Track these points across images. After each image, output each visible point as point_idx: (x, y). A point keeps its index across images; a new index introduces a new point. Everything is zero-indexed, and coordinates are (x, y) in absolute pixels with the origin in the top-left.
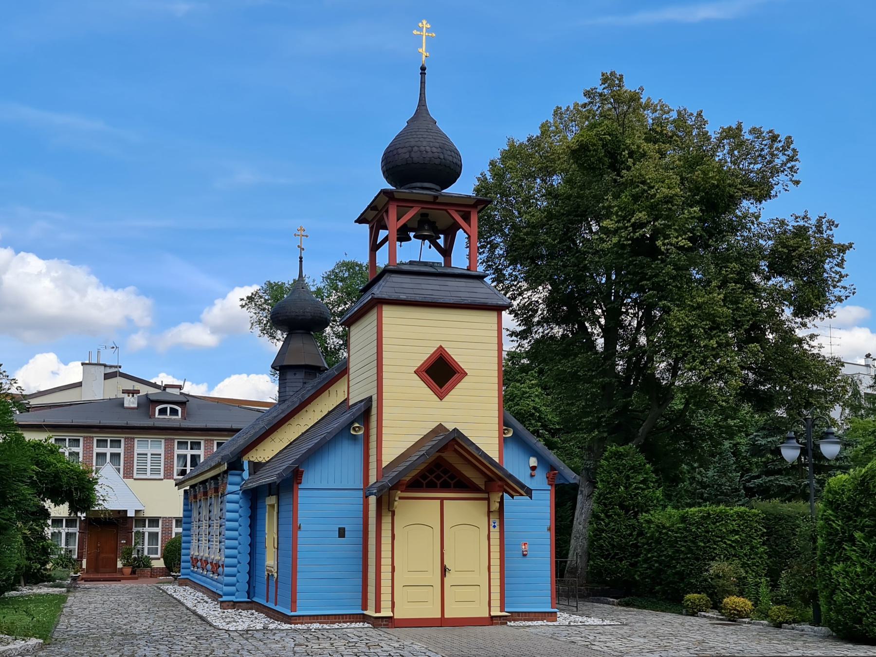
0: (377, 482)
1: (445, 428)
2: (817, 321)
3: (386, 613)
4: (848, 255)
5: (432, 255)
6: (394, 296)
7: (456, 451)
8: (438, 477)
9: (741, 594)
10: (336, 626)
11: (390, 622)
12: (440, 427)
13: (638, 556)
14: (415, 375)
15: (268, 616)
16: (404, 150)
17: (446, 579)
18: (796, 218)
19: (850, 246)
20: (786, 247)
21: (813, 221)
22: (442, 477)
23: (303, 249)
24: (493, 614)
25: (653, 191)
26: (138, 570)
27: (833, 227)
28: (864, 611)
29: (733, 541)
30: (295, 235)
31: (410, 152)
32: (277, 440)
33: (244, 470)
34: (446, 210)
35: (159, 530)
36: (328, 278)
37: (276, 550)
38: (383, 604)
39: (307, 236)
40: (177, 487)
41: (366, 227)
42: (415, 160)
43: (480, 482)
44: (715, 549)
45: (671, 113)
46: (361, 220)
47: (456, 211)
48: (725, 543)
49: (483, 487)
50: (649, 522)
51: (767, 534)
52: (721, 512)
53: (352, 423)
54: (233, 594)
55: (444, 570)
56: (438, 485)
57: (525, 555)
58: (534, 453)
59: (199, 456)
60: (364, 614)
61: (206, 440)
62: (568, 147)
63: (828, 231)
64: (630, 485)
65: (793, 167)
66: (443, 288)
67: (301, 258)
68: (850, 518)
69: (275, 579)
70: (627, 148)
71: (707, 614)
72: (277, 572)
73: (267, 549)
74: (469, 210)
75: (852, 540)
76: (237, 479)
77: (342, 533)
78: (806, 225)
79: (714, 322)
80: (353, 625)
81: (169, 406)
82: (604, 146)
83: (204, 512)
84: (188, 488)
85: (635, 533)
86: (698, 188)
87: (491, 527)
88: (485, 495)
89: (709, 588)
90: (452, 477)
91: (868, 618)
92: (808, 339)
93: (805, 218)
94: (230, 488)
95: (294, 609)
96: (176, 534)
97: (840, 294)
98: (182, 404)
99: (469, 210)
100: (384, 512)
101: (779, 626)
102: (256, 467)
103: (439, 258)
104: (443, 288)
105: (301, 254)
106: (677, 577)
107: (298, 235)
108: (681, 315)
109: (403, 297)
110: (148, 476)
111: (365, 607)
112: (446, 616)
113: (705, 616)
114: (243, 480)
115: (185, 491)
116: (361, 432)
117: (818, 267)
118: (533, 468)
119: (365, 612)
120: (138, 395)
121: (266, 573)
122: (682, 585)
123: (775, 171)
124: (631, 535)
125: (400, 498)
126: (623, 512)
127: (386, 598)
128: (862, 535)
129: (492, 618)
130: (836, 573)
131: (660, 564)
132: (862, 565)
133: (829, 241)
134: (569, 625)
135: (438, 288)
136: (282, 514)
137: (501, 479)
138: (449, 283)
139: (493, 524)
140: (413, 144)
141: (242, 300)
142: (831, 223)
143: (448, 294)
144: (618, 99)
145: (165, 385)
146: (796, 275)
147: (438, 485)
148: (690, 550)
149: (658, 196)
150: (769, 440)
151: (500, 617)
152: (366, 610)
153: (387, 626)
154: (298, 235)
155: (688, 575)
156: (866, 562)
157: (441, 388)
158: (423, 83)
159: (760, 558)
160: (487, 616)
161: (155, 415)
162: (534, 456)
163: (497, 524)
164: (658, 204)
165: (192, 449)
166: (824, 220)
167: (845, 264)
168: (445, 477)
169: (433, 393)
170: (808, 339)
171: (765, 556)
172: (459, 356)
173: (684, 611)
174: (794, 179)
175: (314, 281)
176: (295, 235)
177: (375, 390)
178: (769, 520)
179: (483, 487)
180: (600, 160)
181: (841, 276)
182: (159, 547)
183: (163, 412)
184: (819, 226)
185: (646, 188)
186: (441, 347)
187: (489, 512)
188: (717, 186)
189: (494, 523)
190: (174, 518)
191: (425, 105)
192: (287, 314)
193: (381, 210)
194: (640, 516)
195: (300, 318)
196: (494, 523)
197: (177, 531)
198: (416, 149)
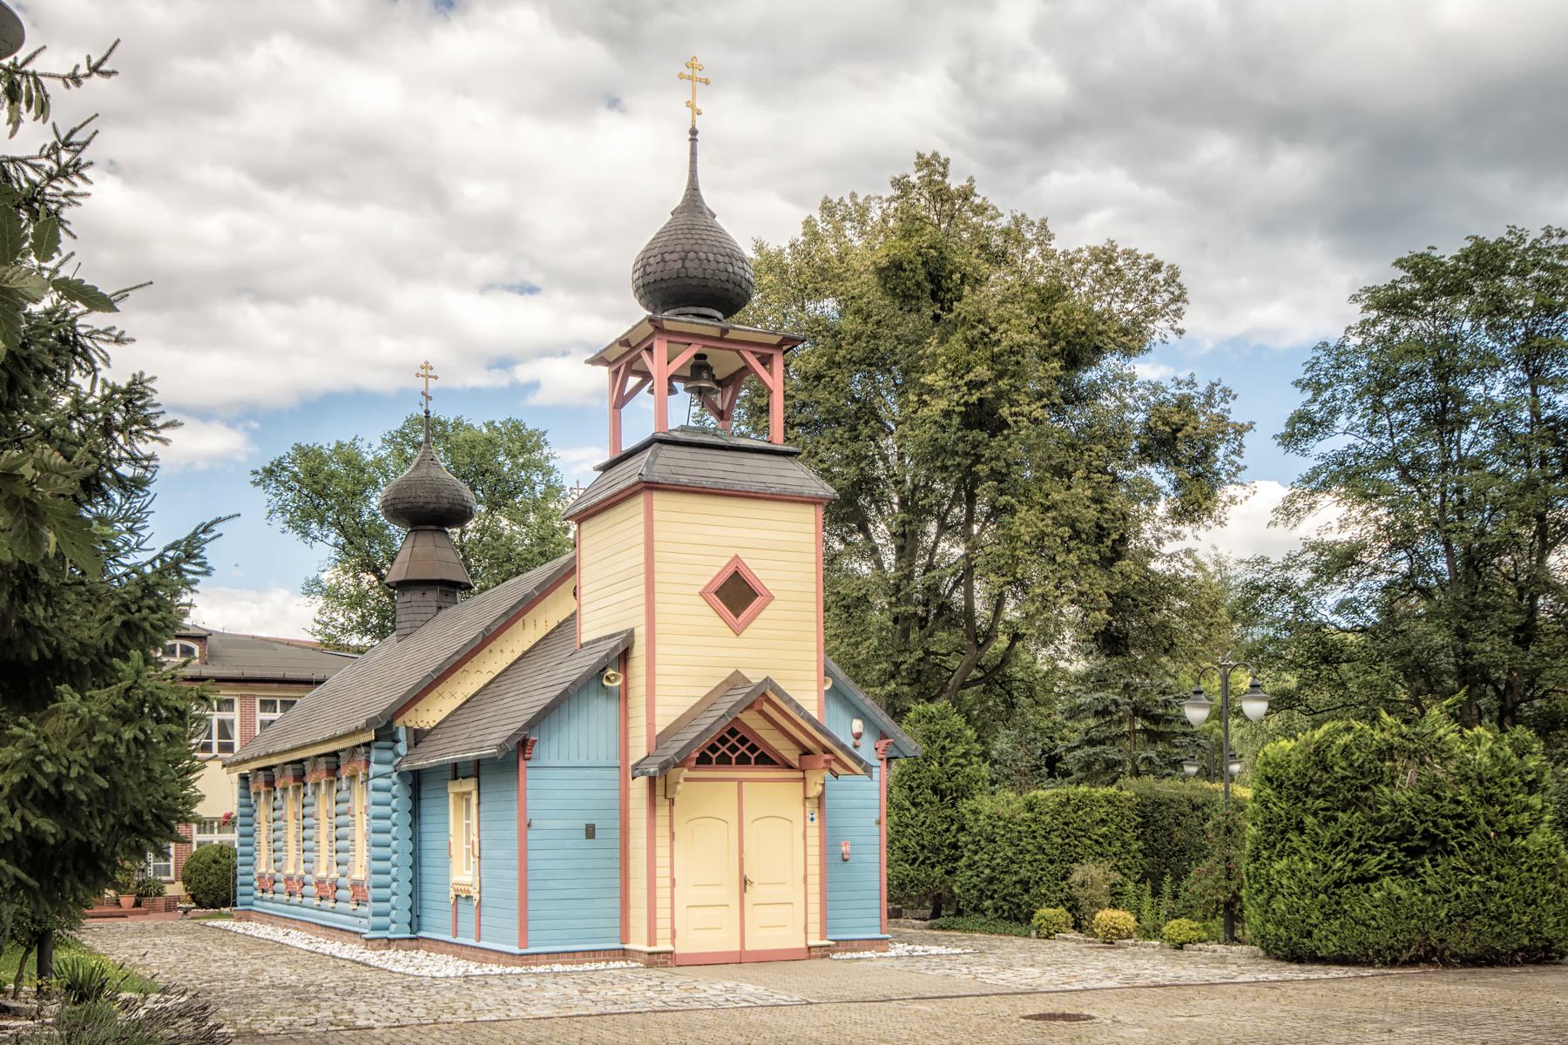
1: (744, 677)
2: (1202, 533)
4: (1248, 438)
6: (672, 479)
7: (762, 713)
8: (733, 749)
9: (1114, 906)
10: (587, 966)
13: (956, 860)
15: (459, 956)
16: (675, 256)
17: (746, 896)
18: (1179, 384)
19: (1251, 426)
20: (1166, 423)
21: (1202, 388)
23: (431, 398)
24: (811, 943)
25: (994, 337)
26: (145, 901)
27: (1229, 399)
28: (1316, 922)
29: (1100, 836)
30: (418, 375)
31: (683, 260)
32: (447, 695)
33: (397, 741)
34: (738, 352)
36: (392, 441)
42: (692, 272)
43: (792, 755)
44: (1076, 846)
45: (1000, 220)
46: (599, 360)
47: (753, 353)
48: (1090, 838)
49: (796, 763)
50: (975, 812)
51: (1143, 825)
52: (1084, 796)
53: (604, 669)
55: (745, 882)
56: (734, 761)
57: (845, 860)
58: (861, 715)
59: (232, 722)
60: (624, 949)
61: (242, 696)
62: (874, 263)
63: (1223, 405)
64: (947, 760)
65: (1179, 309)
66: (738, 469)
67: (694, 132)
68: (1298, 799)
69: (475, 903)
70: (957, 269)
71: (1068, 936)
73: (453, 860)
74: (769, 351)
75: (1300, 828)
76: (389, 755)
77: (590, 832)
78: (1193, 393)
79: (1072, 527)
80: (612, 965)
81: (178, 643)
82: (924, 264)
83: (845, 794)
85: (954, 828)
86: (1055, 335)
87: (808, 821)
88: (800, 775)
89: (1068, 900)
90: (753, 749)
91: (1320, 930)
92: (1182, 556)
93: (1191, 383)
94: (375, 768)
96: (199, 844)
97: (1236, 493)
99: (769, 351)
100: (659, 799)
101: (1180, 947)
104: (738, 469)
106: (1018, 886)
108: (1032, 515)
109: (684, 480)
111: (625, 937)
112: (748, 948)
113: (1066, 939)
114: (397, 755)
116: (617, 683)
117: (1206, 454)
119: (626, 946)
121: (452, 894)
122: (1026, 898)
123: (1154, 312)
124: (948, 830)
125: (686, 780)
126: (936, 799)
127: (663, 924)
128: (1315, 821)
130: (1278, 872)
131: (993, 870)
132: (1314, 860)
133: (1222, 419)
135: (731, 468)
136: (482, 809)
137: (827, 751)
138: (745, 461)
140: (688, 247)
141: (256, 473)
142: (1227, 394)
143: (746, 477)
144: (941, 195)
146: (1178, 463)
147: (734, 761)
148: (1041, 849)
149: (1005, 343)
150: (1097, 695)
153: (665, 965)
155: (1037, 883)
156: (1321, 856)
157: (737, 616)
158: (693, 154)
159: (1134, 857)
160: (803, 945)
164: (1002, 355)
165: (219, 710)
166: (1217, 389)
167: (1246, 452)
169: (724, 624)
170: (1182, 556)
171: (1140, 856)
172: (761, 571)
173: (1034, 933)
174: (1176, 327)
175: (370, 446)
176: (418, 375)
177: (642, 620)
178: (1145, 806)
180: (918, 284)
181: (1239, 469)
184: (1210, 396)
185: (987, 330)
186: (737, 556)
188: (1084, 333)
192: (412, 500)
193: (639, 345)
194: (959, 803)
195: (432, 506)
198: (692, 255)
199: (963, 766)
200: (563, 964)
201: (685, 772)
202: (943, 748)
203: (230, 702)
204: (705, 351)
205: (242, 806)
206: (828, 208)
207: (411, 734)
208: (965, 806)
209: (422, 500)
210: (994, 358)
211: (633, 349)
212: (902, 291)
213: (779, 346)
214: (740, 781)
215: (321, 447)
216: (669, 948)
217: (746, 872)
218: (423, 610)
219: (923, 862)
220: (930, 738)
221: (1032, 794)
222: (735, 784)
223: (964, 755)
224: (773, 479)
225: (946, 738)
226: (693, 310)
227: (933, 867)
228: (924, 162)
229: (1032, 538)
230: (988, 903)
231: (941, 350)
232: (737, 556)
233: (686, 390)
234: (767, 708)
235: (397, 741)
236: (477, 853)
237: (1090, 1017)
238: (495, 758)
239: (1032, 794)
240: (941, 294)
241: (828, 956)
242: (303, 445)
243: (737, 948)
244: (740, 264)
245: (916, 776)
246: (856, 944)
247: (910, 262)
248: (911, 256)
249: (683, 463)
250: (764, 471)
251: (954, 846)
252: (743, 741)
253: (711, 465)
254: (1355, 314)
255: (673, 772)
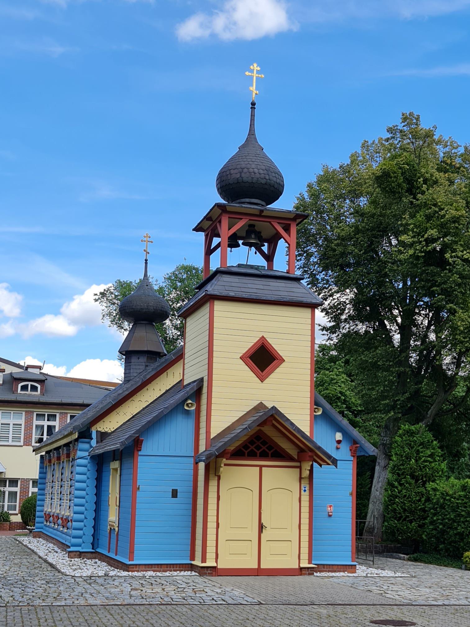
0: (206, 450)
3: (210, 563)
5: (258, 260)
6: (224, 293)
7: (274, 426)
8: (258, 448)
10: (167, 574)
11: (213, 571)
12: (261, 406)
13: (425, 519)
14: (241, 360)
16: (236, 171)
17: (262, 535)
22: (261, 448)
24: (302, 566)
25: (442, 213)
31: (241, 173)
33: (92, 439)
34: (270, 222)
35: (17, 489)
36: (169, 278)
37: (118, 508)
38: (208, 556)
39: (152, 242)
40: (34, 452)
41: (201, 236)
42: (245, 179)
43: (293, 452)
45: (459, 149)
47: (279, 223)
49: (296, 457)
50: (435, 490)
53: (186, 400)
54: (80, 546)
55: (261, 527)
56: (258, 455)
57: (330, 516)
60: (192, 564)
61: (60, 413)
64: (420, 458)
66: (265, 287)
67: (146, 260)
72: (118, 527)
73: (110, 507)
76: (86, 446)
77: (175, 494)
81: (30, 384)
84: (44, 453)
87: (302, 491)
90: (270, 448)
95: (131, 559)
96: (33, 493)
98: (41, 382)
102: (103, 436)
103: (263, 262)
104: (265, 287)
105: (146, 257)
107: (145, 241)
110: (10, 443)
111: (193, 558)
112: (262, 567)
114: (91, 447)
115: (42, 457)
118: (339, 442)
119: (193, 562)
120: (4, 373)
121: (109, 527)
122: (462, 544)
124: (420, 500)
125: (225, 465)
126: (413, 482)
127: (211, 549)
129: (301, 569)
131: (444, 526)
134: (367, 577)
135: (262, 287)
138: (271, 284)
139: (304, 489)
143: (270, 292)
145: (27, 365)
147: (258, 455)
149: (447, 216)
151: (308, 568)
152: (194, 560)
154: (145, 241)
157: (262, 372)
158: (253, 116)
160: (297, 567)
161: (17, 391)
162: (339, 431)
163: (307, 489)
165: (48, 420)
168: (264, 448)
173: (463, 566)
179: (296, 457)
180: (399, 185)
182: (18, 504)
183: (24, 388)
186: (263, 337)
187: (301, 478)
189: (305, 488)
190: (31, 479)
191: (254, 134)
194: (427, 485)
195: (144, 310)
196: (305, 488)
197: (33, 491)
198: (245, 170)
199: (430, 462)
200: (154, 571)
201: (224, 461)
202: (418, 451)
203: (55, 416)
204: (252, 222)
205: (40, 473)
206: (365, 145)
207: (99, 435)
208: (430, 485)
209: (139, 307)
210: (442, 226)
211: (214, 222)
212: (390, 189)
213: (294, 219)
214: (261, 467)
215: (131, 282)
216: (214, 564)
217: (262, 521)
218: (138, 367)
219: (405, 520)
220: (410, 445)
221: (466, 481)
222: (258, 468)
223: (432, 456)
224: (286, 294)
225: (419, 446)
226: (247, 200)
227: (411, 522)
228: (406, 119)
229: (465, 329)
230: (441, 546)
231: (411, 221)
232: (263, 337)
233: (243, 244)
234: (274, 422)
235: (92, 439)
236: (118, 504)
237: (371, 622)
238: (119, 449)
239: (466, 481)
240: (414, 190)
241: (313, 574)
242: (121, 281)
243: (256, 567)
244: (274, 175)
245: (402, 467)
246: (336, 567)
247: (395, 173)
248: (395, 169)
249: (233, 284)
250: (281, 289)
251: (424, 510)
252: (264, 443)
253: (250, 286)
254: (337, 167)
255: (219, 459)
